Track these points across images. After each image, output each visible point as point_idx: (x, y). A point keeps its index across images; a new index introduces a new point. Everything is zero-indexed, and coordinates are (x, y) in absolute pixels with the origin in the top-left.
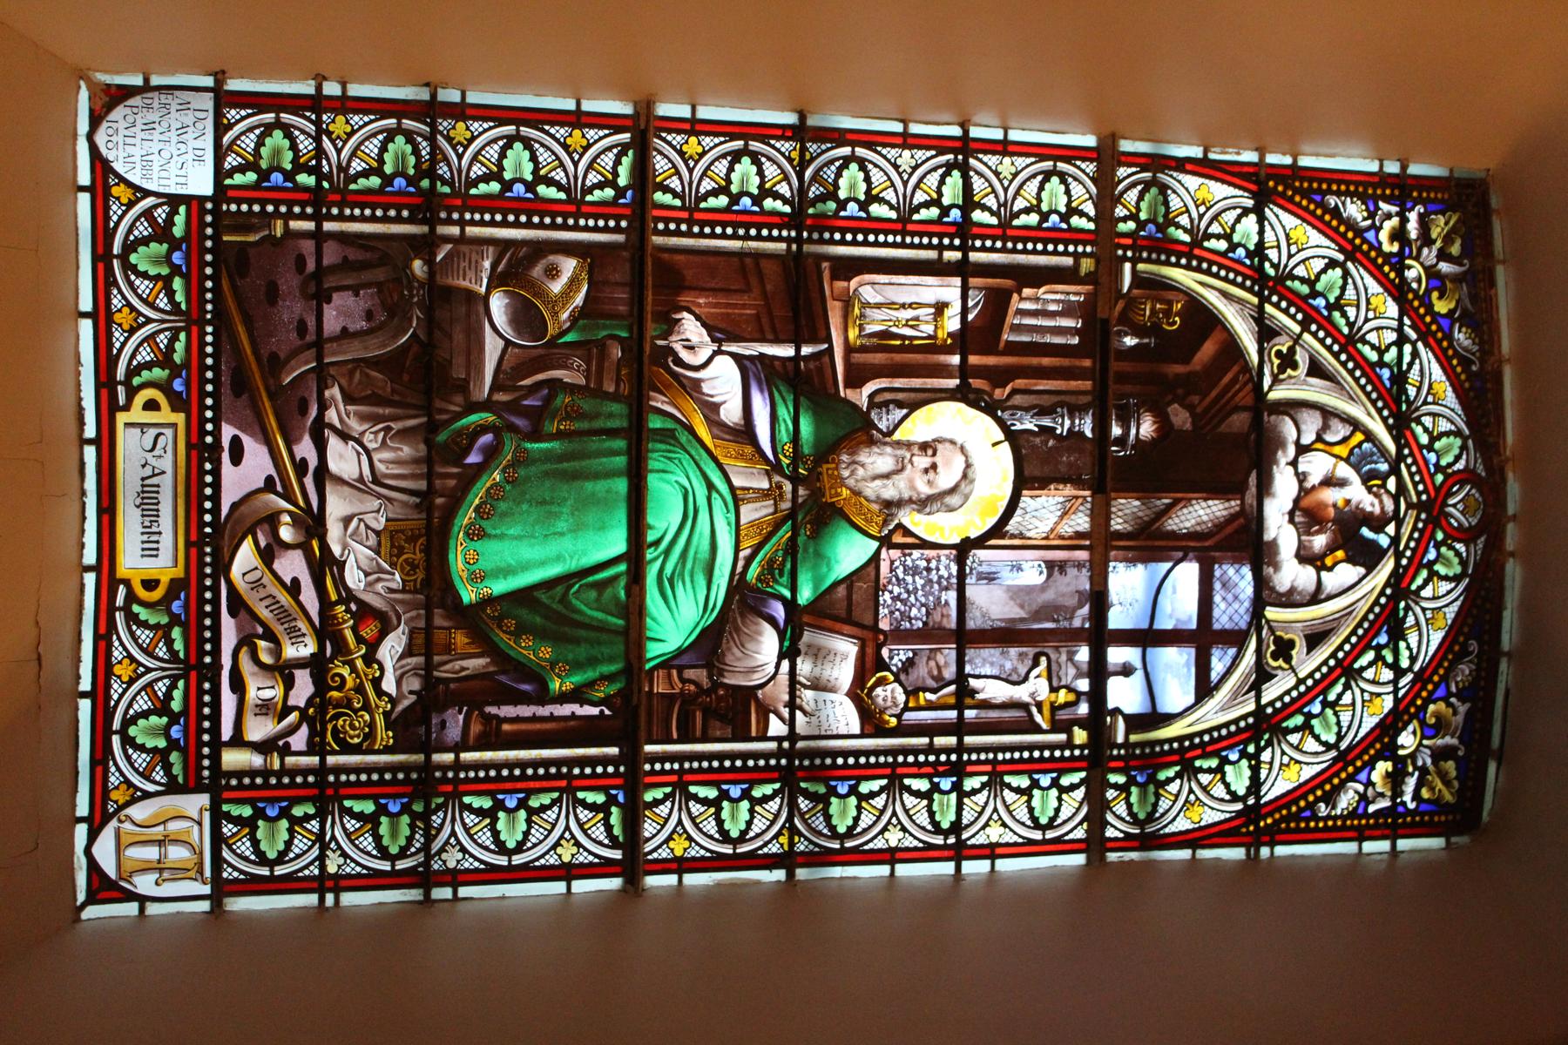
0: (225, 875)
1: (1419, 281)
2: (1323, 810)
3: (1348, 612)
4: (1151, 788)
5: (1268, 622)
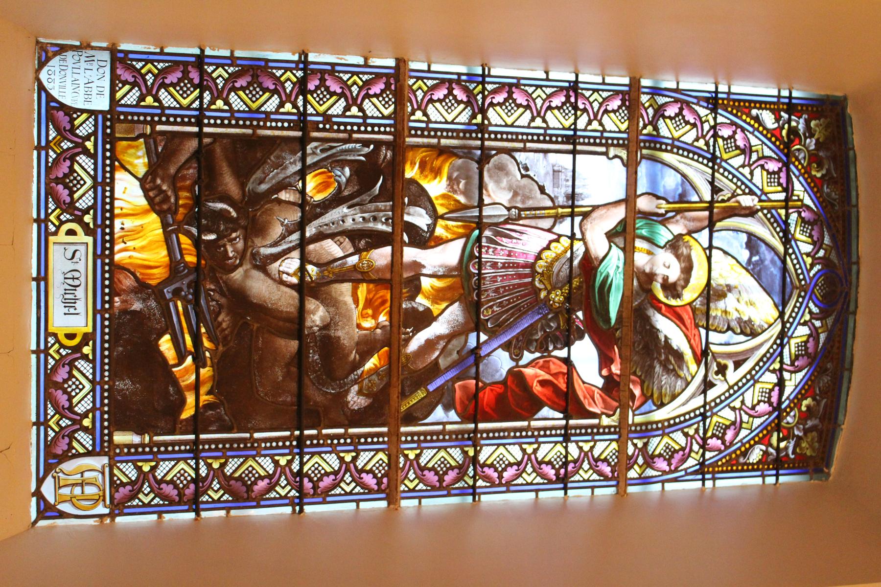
5: (713, 354)
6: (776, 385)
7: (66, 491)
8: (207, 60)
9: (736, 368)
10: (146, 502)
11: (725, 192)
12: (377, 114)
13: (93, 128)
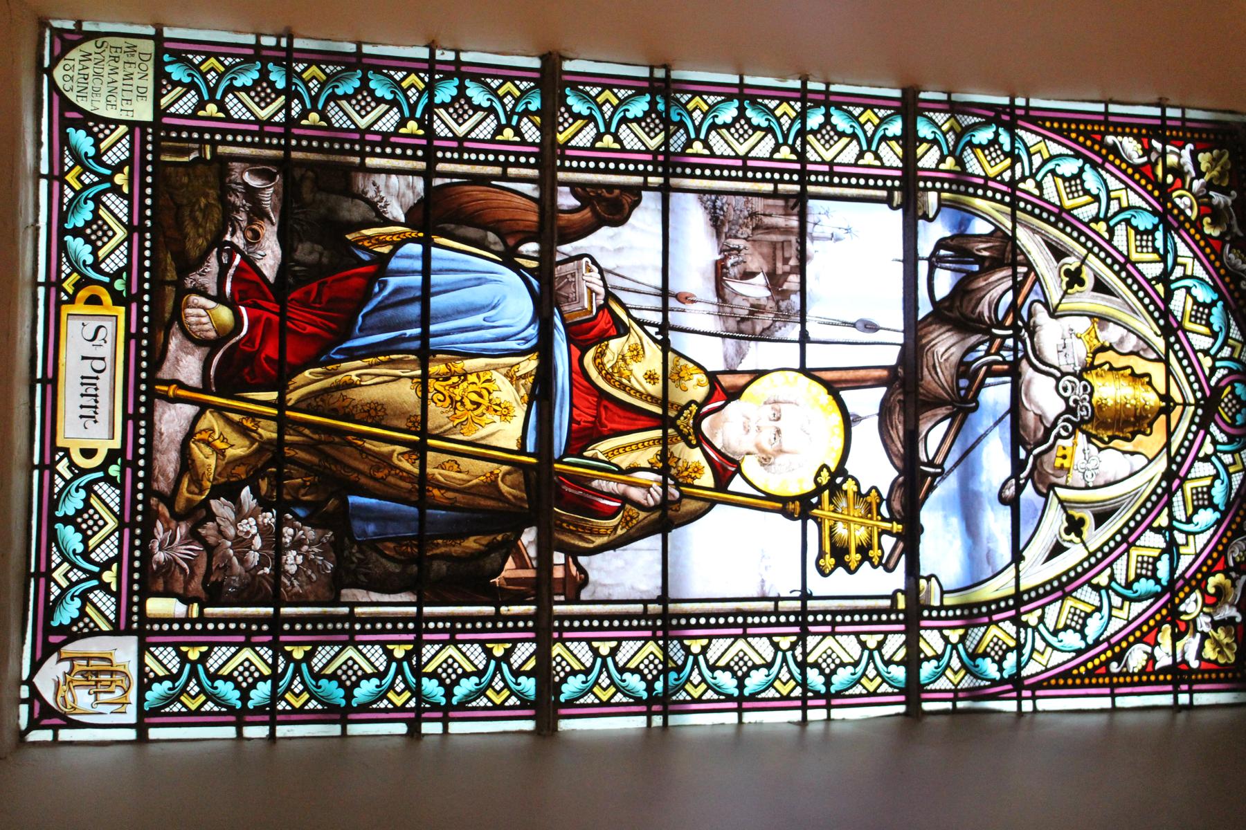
1: (1191, 208)
2: (1114, 667)
3: (1136, 493)
6: (1164, 551)
8: (295, 55)
9: (1098, 525)
10: (193, 707)
12: (639, 146)
13: (127, 154)
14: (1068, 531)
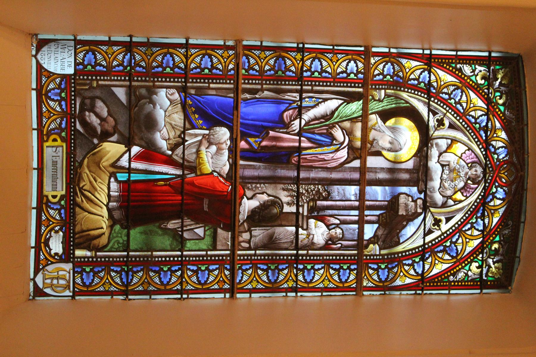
0: (365, 284)
4: (312, 271)
7: (48, 281)
9: (447, 222)
11: (440, 114)
14: (434, 225)
